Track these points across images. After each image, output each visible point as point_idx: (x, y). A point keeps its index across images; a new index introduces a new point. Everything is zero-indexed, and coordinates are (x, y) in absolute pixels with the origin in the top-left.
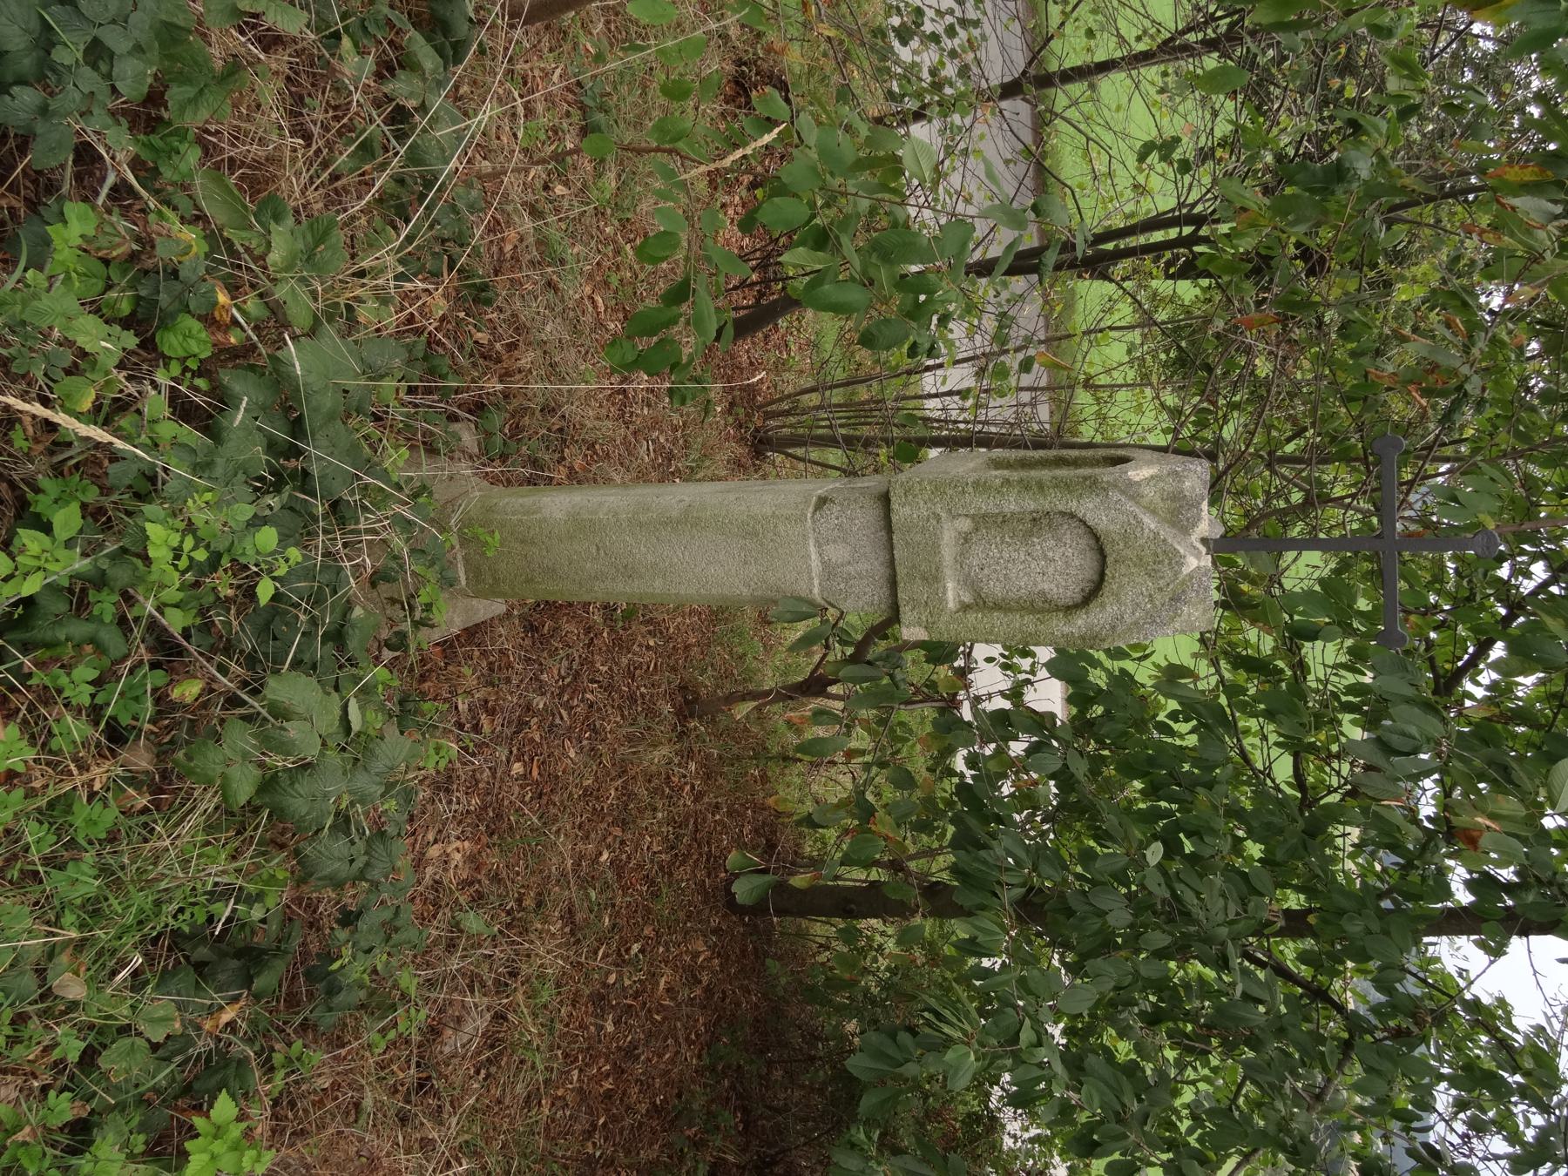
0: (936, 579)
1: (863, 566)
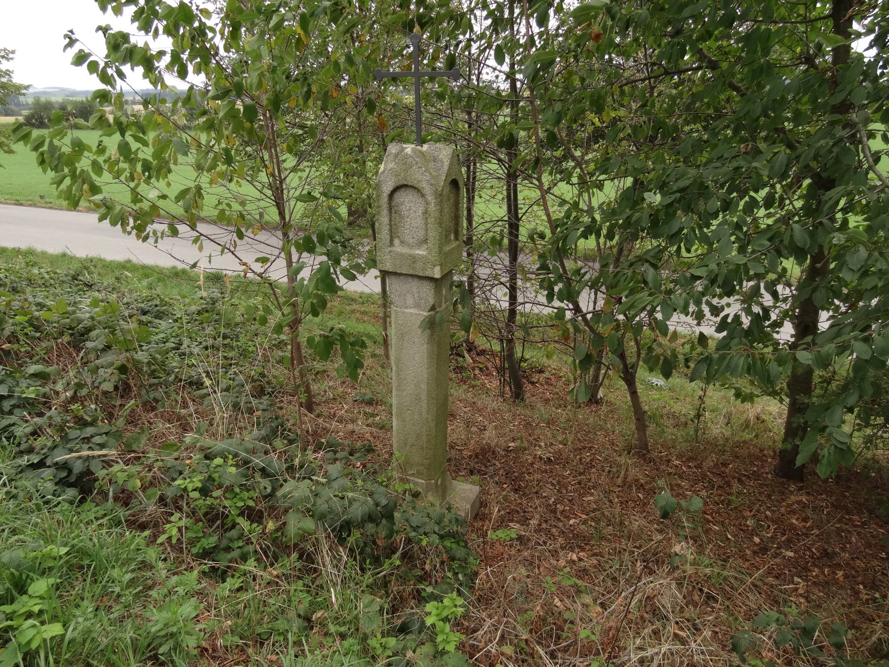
0: (414, 257)
1: (415, 290)
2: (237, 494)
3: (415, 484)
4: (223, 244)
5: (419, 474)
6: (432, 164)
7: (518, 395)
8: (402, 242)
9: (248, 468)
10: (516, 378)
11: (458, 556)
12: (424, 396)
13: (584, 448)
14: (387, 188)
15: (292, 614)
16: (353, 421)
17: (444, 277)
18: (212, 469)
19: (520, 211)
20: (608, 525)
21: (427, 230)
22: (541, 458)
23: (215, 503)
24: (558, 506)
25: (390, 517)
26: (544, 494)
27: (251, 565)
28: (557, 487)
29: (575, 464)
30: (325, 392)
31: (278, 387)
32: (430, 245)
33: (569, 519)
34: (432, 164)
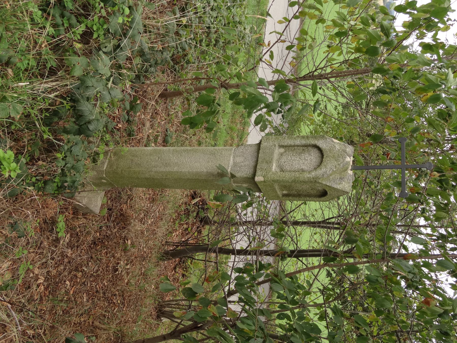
0: (270, 162)
1: (247, 163)
2: (102, 26)
3: (103, 163)
4: (284, 34)
5: (110, 165)
6: (338, 176)
7: (167, 255)
8: (282, 154)
9: (121, 36)
10: (180, 254)
11: (47, 187)
12: (168, 169)
13: (124, 299)
14: (321, 144)
15: (12, 53)
16: (152, 126)
17: (255, 184)
18: (121, 6)
19: (304, 258)
20: (63, 311)
21: (290, 171)
22: (118, 263)
23: (97, 10)
24: (81, 273)
25: (79, 132)
26: (90, 263)
27: (50, 30)
28: (95, 274)
29: (112, 289)
30: (175, 109)
31: (179, 75)
32: (279, 173)
33: (70, 281)
34: (338, 176)
